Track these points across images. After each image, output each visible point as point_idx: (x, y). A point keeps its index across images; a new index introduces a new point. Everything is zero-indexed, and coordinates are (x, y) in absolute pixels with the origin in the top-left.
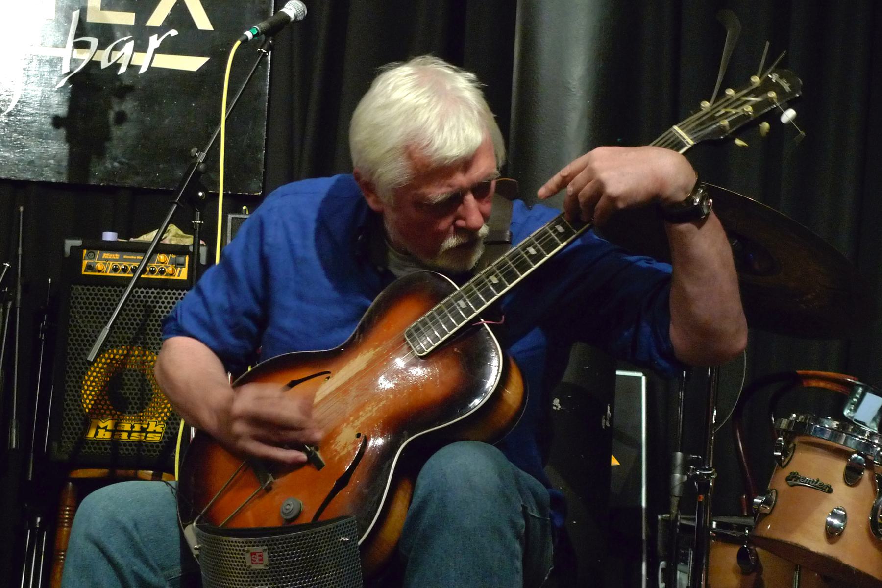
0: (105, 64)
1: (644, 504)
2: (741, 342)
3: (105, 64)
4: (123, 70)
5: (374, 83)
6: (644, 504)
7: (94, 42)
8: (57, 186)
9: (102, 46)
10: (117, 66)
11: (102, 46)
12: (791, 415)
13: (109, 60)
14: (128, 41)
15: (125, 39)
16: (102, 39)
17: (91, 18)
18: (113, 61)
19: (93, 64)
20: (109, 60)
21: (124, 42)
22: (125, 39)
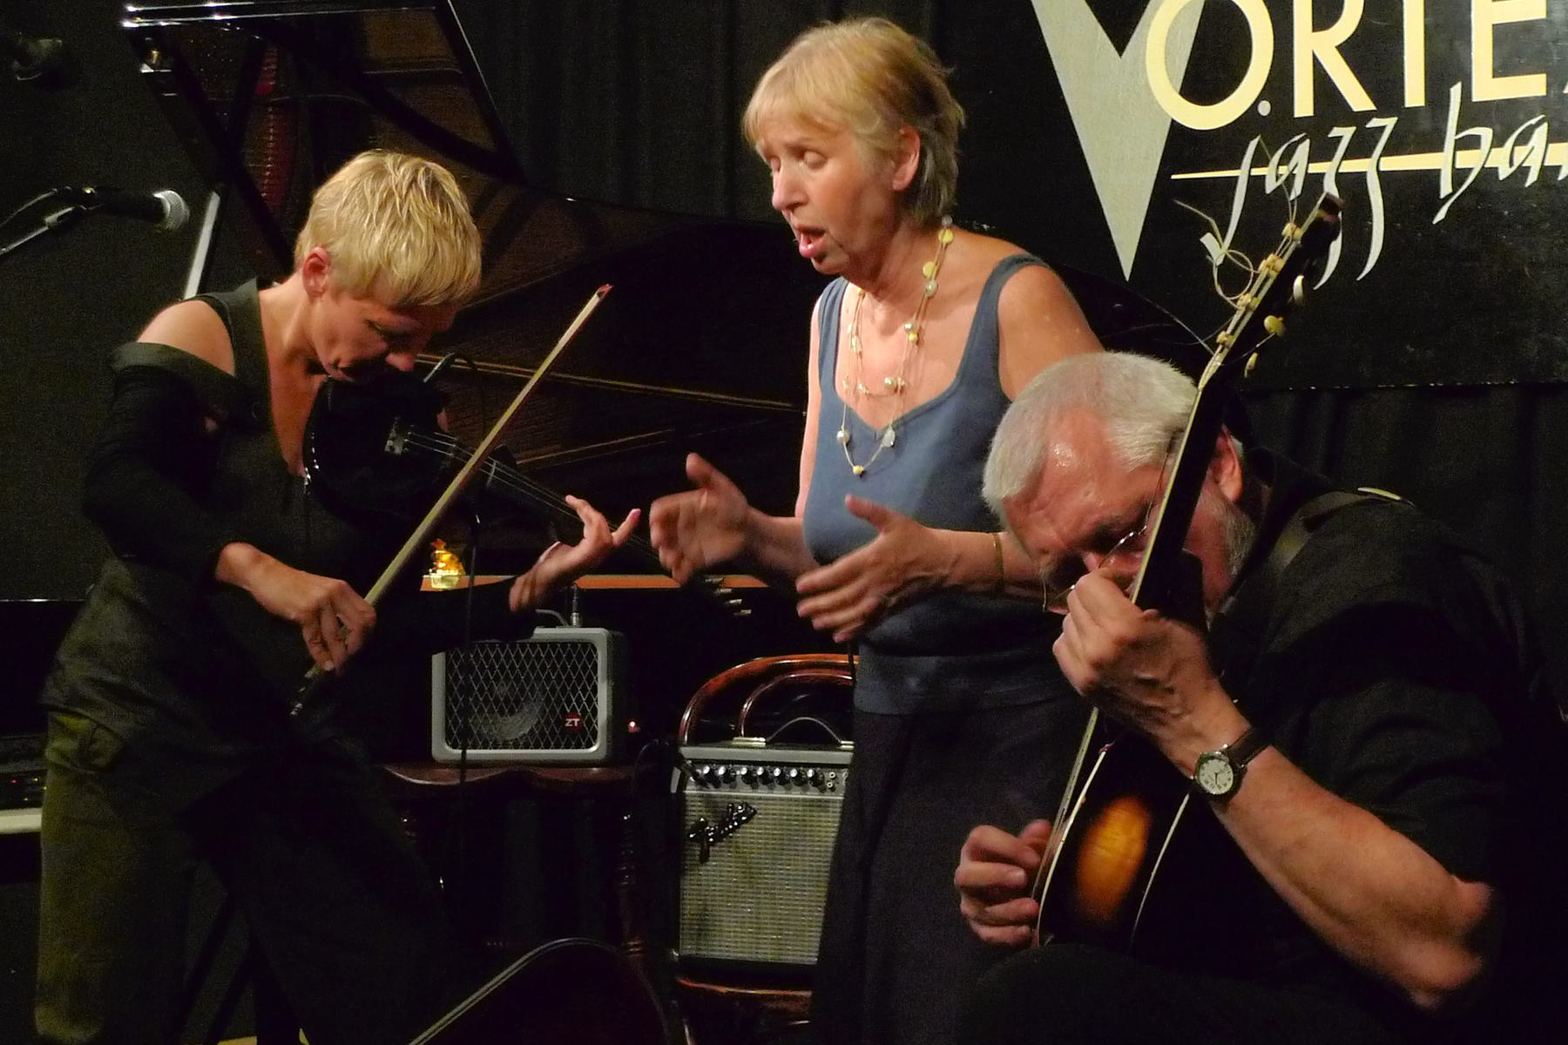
0: (1505, 172)
1: (594, 301)
2: (1216, 812)
3: (1505, 172)
4: (1532, 178)
5: (258, 598)
6: (594, 301)
7: (1486, 134)
8: (1072, 692)
9: (1498, 142)
10: (1523, 171)
11: (1498, 142)
12: (151, 56)
13: (1511, 164)
14: (1539, 124)
15: (1533, 121)
16: (1498, 127)
17: (1478, 96)
18: (1516, 164)
19: (1488, 173)
20: (1511, 164)
21: (1532, 129)
22: (1533, 121)
